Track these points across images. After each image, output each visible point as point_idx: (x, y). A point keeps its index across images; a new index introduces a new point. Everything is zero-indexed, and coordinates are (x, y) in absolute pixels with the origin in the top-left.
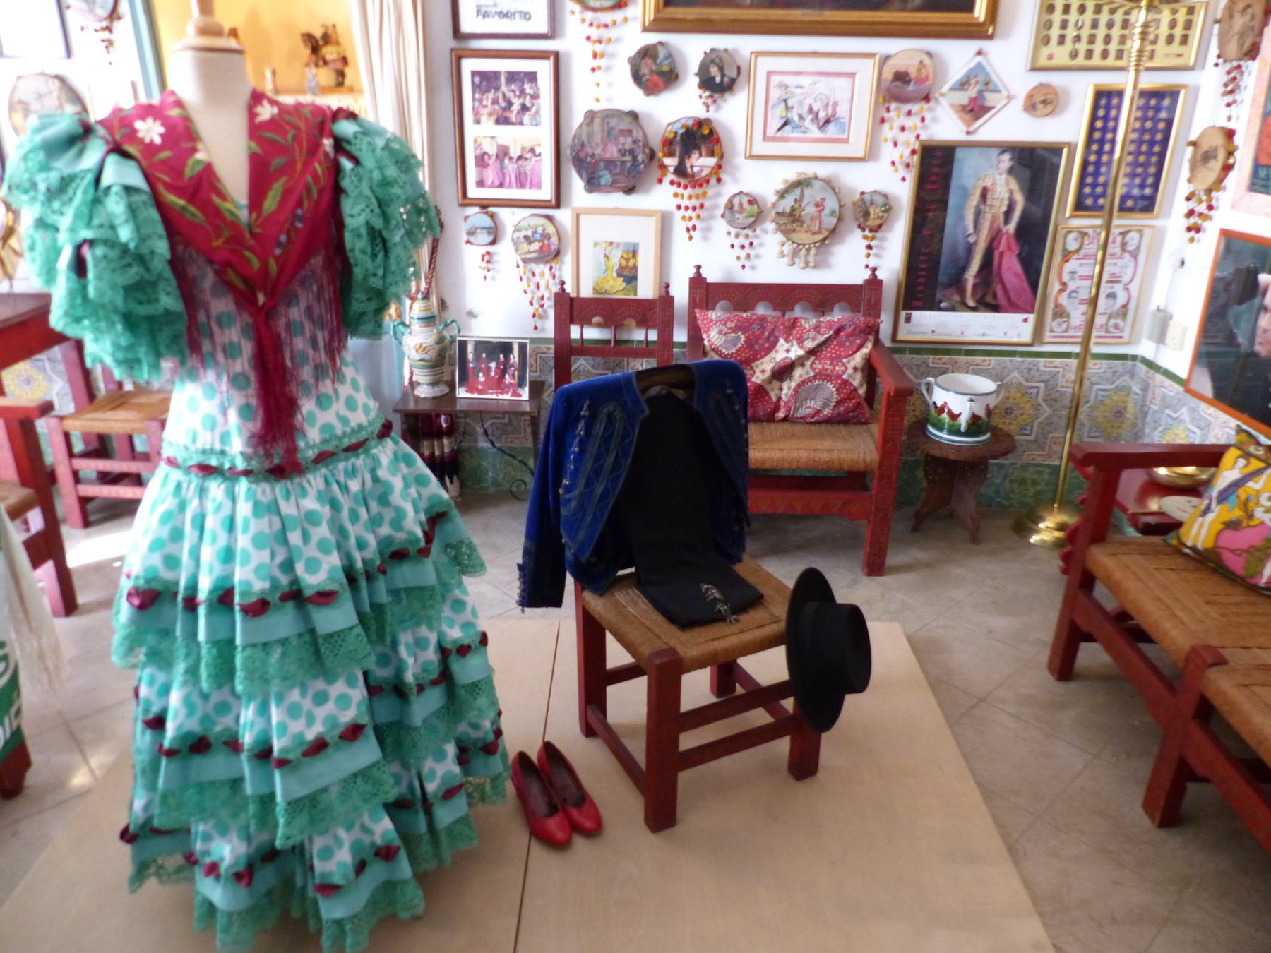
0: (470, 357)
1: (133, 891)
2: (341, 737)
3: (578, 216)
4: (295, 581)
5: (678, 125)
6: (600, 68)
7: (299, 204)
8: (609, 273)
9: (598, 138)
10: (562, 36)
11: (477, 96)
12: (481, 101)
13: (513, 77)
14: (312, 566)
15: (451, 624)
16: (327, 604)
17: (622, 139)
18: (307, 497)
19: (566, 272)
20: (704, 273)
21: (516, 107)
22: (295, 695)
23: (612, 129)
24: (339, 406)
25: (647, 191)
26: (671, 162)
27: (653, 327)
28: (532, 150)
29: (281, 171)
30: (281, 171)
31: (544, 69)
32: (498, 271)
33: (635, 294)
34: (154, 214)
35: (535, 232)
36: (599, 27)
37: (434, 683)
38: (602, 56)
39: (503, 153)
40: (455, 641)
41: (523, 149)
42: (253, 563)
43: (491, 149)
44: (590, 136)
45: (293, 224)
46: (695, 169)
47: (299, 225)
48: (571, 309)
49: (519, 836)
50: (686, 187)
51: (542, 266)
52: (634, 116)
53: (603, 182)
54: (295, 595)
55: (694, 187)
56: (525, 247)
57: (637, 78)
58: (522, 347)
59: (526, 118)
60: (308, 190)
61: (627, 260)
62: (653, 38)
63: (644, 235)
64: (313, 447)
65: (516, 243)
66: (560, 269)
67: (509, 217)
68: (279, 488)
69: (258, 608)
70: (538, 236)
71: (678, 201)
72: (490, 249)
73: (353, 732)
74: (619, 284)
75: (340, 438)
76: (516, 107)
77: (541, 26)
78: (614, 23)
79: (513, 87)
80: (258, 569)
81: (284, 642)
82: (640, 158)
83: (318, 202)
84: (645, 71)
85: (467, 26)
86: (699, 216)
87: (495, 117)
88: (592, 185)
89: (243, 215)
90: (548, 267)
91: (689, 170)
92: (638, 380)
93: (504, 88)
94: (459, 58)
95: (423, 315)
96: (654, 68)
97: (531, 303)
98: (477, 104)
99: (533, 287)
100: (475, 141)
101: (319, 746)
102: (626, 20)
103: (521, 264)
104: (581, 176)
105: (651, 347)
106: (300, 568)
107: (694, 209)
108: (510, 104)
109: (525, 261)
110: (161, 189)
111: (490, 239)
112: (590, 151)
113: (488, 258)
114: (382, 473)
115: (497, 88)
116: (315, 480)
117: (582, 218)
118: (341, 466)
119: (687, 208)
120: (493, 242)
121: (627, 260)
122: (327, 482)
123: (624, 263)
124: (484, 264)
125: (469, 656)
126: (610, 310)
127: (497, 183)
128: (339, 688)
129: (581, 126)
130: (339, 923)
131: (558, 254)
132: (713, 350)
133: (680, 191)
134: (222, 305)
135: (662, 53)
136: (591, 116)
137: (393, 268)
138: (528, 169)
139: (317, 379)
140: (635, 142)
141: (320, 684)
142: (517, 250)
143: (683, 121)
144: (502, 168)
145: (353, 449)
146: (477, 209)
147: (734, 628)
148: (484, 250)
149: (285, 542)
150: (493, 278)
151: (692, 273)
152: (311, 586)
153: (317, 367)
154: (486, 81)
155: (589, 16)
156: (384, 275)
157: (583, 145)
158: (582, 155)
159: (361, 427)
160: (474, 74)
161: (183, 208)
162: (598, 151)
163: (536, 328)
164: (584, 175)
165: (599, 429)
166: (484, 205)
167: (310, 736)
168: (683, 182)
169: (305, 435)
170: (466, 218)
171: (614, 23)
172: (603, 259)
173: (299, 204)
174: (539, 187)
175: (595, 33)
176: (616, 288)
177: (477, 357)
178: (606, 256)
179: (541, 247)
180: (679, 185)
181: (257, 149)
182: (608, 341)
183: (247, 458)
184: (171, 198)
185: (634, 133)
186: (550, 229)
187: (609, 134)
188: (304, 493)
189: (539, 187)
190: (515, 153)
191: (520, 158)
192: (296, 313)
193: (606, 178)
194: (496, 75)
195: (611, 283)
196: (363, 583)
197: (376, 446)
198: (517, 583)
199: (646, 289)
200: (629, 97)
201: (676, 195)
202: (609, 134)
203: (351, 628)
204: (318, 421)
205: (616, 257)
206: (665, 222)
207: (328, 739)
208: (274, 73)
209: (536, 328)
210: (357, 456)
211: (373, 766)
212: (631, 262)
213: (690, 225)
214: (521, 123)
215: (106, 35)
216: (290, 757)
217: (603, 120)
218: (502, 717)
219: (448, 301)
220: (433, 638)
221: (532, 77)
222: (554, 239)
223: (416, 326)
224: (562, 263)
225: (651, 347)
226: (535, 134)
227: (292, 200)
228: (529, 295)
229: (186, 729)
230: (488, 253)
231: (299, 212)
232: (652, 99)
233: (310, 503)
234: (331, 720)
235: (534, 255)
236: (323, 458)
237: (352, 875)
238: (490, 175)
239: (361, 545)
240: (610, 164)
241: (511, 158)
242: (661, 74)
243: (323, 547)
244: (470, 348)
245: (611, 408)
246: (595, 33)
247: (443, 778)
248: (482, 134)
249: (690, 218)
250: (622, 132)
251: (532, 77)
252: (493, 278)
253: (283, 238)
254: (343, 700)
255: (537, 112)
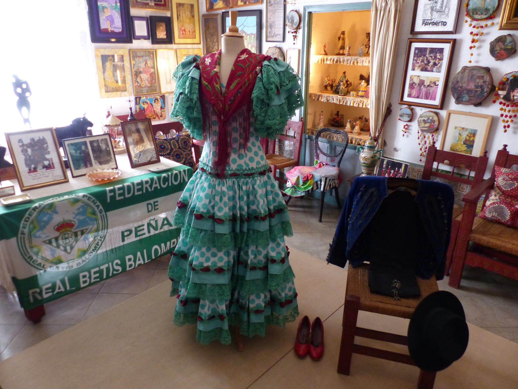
0: (384, 166)
1: (171, 296)
2: (215, 270)
3: (450, 114)
4: (214, 213)
5: (510, 75)
6: (474, 47)
7: (241, 88)
8: (459, 142)
9: (466, 80)
10: (460, 32)
11: (415, 58)
12: (416, 60)
13: (432, 50)
14: (220, 209)
15: (273, 250)
16: (219, 223)
17: (478, 80)
18: (224, 187)
19: (440, 138)
20: (508, 149)
21: (431, 64)
22: (204, 250)
23: (474, 75)
24: (247, 160)
25: (488, 106)
26: (502, 93)
27: (474, 170)
28: (435, 83)
29: (239, 76)
30: (239, 76)
31: (447, 47)
32: (410, 133)
33: (471, 154)
34: (197, 86)
35: (429, 119)
36: (478, 28)
37: (260, 269)
38: (477, 41)
39: (422, 83)
40: (271, 257)
41: (431, 82)
42: (203, 203)
43: (416, 81)
44: (462, 78)
45: (237, 94)
46: (515, 97)
47: (239, 95)
48: (434, 154)
49: (290, 346)
50: (508, 106)
51: (429, 134)
52: (488, 70)
53: (464, 100)
54: (212, 217)
55: (512, 106)
56: (423, 125)
57: (493, 51)
58: (406, 166)
59: (435, 69)
60: (245, 83)
61: (470, 137)
62: (505, 33)
63: (481, 127)
64: (232, 170)
65: (419, 122)
66: (437, 137)
67: (419, 111)
68: (217, 182)
69: (200, 217)
70: (429, 121)
71: (503, 112)
72: (408, 123)
73: (220, 270)
74: (464, 148)
75: (244, 170)
76: (431, 64)
77: (450, 27)
78: (486, 26)
79: (432, 55)
80: (203, 205)
81: (206, 231)
82: (485, 90)
83: (247, 88)
84: (497, 48)
85: (419, 27)
86: (512, 121)
87: (421, 68)
88: (459, 101)
89: (224, 90)
90: (431, 135)
91: (512, 97)
92: (388, 182)
93: (427, 55)
94: (411, 43)
95: (369, 145)
96: (503, 47)
97: (421, 149)
98: (415, 62)
99: (423, 142)
100: (411, 78)
101: (207, 270)
102: (493, 24)
103: (420, 131)
104: (454, 97)
105: (470, 179)
106: (216, 208)
107: (511, 117)
108: (429, 62)
109: (422, 131)
110: (202, 79)
111: (409, 119)
112: (460, 84)
113: (407, 128)
114: (256, 186)
115: (425, 55)
116: (229, 182)
117: (452, 115)
118: (242, 180)
119: (506, 116)
120: (410, 121)
121: (470, 137)
122: (234, 183)
123: (468, 138)
124: (404, 130)
125: (274, 264)
126: (453, 158)
127: (416, 96)
128: (221, 254)
129: (459, 73)
130: (201, 331)
131: (437, 130)
132: (498, 187)
133: (504, 107)
134: (214, 118)
135: (509, 39)
136: (465, 68)
137: (269, 114)
138: (431, 91)
139: (240, 149)
140: (484, 82)
141: (214, 250)
142: (419, 125)
143: (514, 73)
144: (420, 90)
145: (248, 175)
146: (406, 106)
147: (394, 302)
148: (405, 124)
149: (214, 199)
150: (407, 136)
151: (501, 148)
152: (217, 216)
153: (240, 144)
154: (421, 52)
155: (474, 23)
156: (265, 116)
157: (458, 82)
158: (457, 86)
159: (253, 168)
160: (416, 49)
161: (207, 85)
162: (464, 85)
163: (421, 160)
164: (456, 95)
165: (366, 198)
166: (410, 105)
167: (205, 265)
168: (507, 103)
169: (229, 166)
170: (401, 109)
171: (486, 26)
172: (458, 135)
173: (241, 88)
174: (435, 99)
175: (475, 31)
176: (462, 149)
177: (387, 167)
178: (460, 134)
179: (430, 126)
180: (504, 104)
181: (234, 69)
182: (450, 172)
183: (211, 169)
184: (204, 82)
185: (485, 78)
186: (436, 118)
187: (472, 77)
188: (224, 185)
189: (435, 99)
190: (427, 83)
191: (429, 86)
192: (235, 125)
193: (466, 98)
194: (425, 49)
195: (460, 147)
196: (238, 222)
197: (257, 177)
198: (328, 252)
199: (477, 152)
200: (486, 60)
201: (502, 109)
202: (472, 78)
203: (225, 234)
204: (236, 162)
205: (465, 135)
206: (493, 122)
207: (211, 268)
208: (349, 48)
209: (421, 160)
210: (249, 178)
211: (224, 285)
212: (472, 139)
213: (507, 124)
214: (432, 71)
215: (294, 34)
216: (196, 268)
217: (470, 70)
218: (298, 297)
219: (387, 142)
220: (264, 252)
221: (441, 50)
222: (437, 123)
223: (366, 150)
224: (439, 134)
225: (470, 179)
226: (440, 76)
227: (239, 86)
228: (421, 146)
229: (182, 249)
230: (407, 125)
231: (240, 90)
232: (499, 62)
233: (224, 189)
234: (215, 263)
235: (426, 129)
236: (234, 175)
237: (207, 318)
238: (414, 92)
239: (241, 208)
240: (469, 91)
241: (425, 86)
242: (506, 50)
243: (225, 204)
244: (385, 163)
245: (373, 190)
246: (475, 31)
247: (257, 305)
248: (414, 74)
249: (507, 121)
250: (479, 77)
251: (441, 50)
252: (407, 136)
253: (232, 98)
254: (221, 259)
255: (440, 67)
